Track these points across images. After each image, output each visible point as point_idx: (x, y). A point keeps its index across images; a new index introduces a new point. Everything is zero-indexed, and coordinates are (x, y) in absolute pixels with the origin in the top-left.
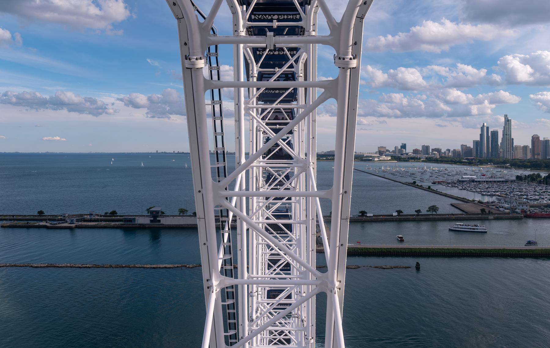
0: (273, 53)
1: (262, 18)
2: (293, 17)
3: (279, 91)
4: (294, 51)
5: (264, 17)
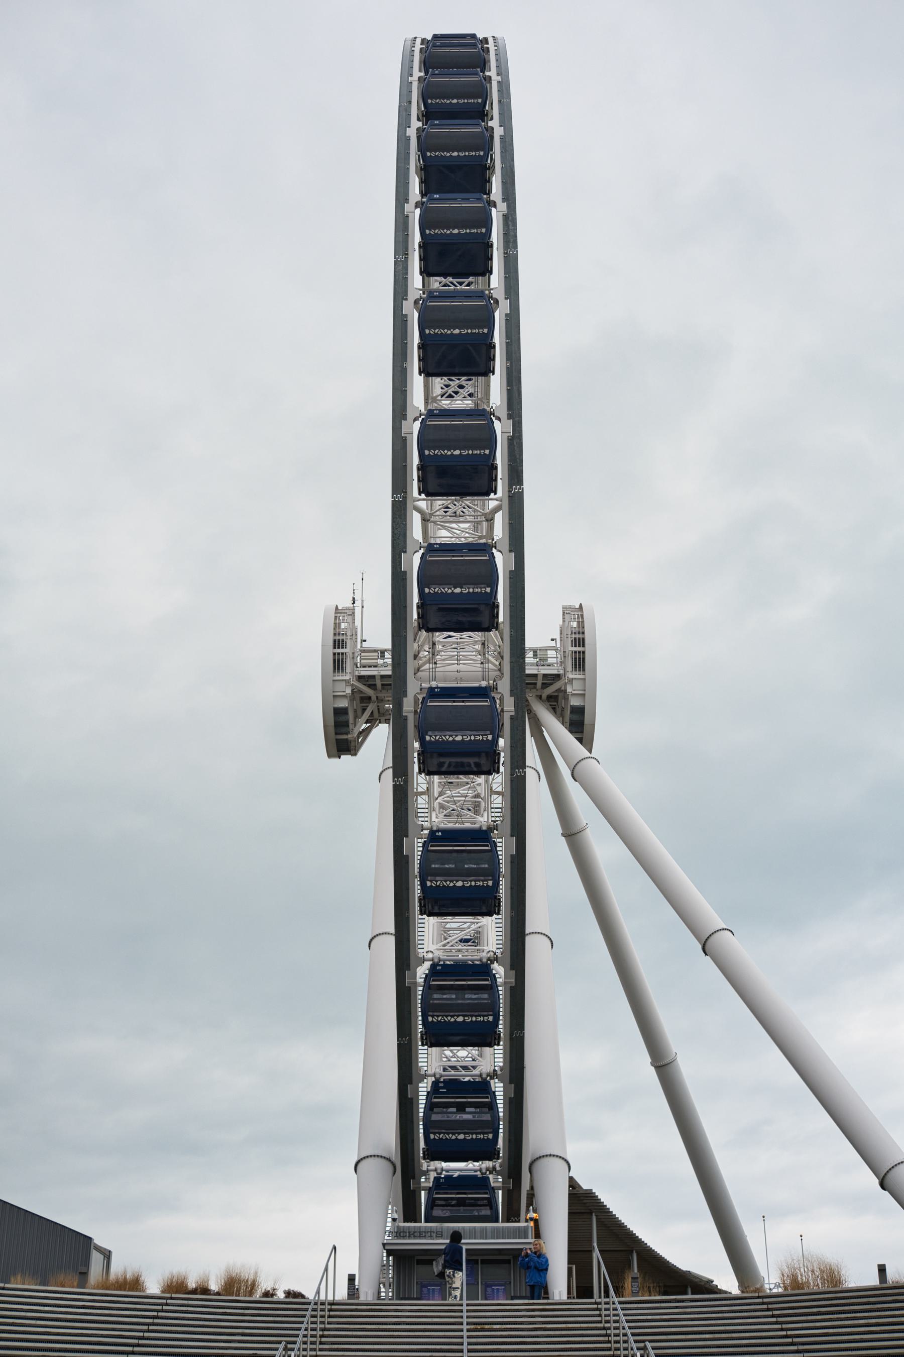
0: (457, 1137)
1: (441, 885)
3: (458, 100)
4: (486, 450)
5: (444, 1019)
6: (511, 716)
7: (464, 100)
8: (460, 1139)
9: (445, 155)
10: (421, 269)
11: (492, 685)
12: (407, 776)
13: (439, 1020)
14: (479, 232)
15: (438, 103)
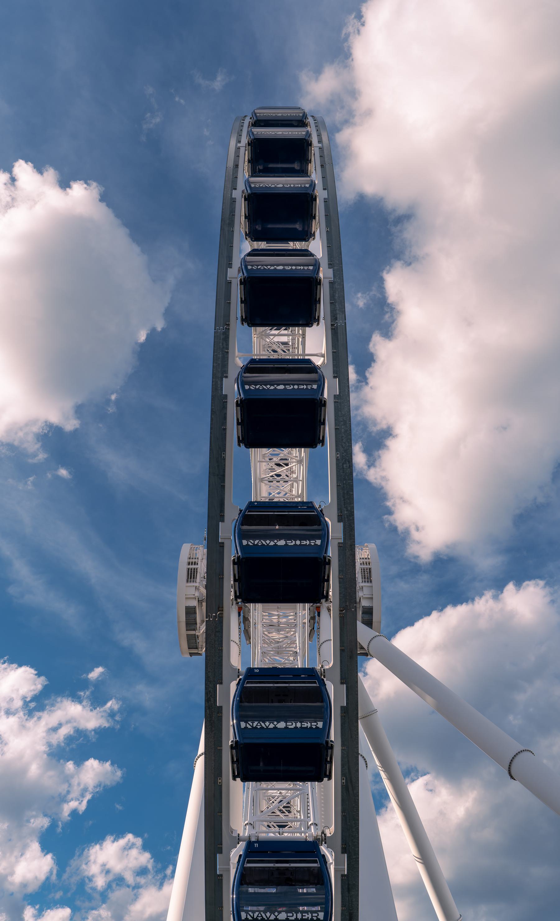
0: (275, 725)
1: (259, 727)
2: (311, 725)
3: (286, 722)
5: (261, 725)
6: (339, 543)
7: (295, 541)
8: (279, 728)
9: (268, 389)
10: (239, 437)
11: (321, 838)
12: (223, 611)
13: (254, 726)
14: (313, 544)
15: (260, 269)
